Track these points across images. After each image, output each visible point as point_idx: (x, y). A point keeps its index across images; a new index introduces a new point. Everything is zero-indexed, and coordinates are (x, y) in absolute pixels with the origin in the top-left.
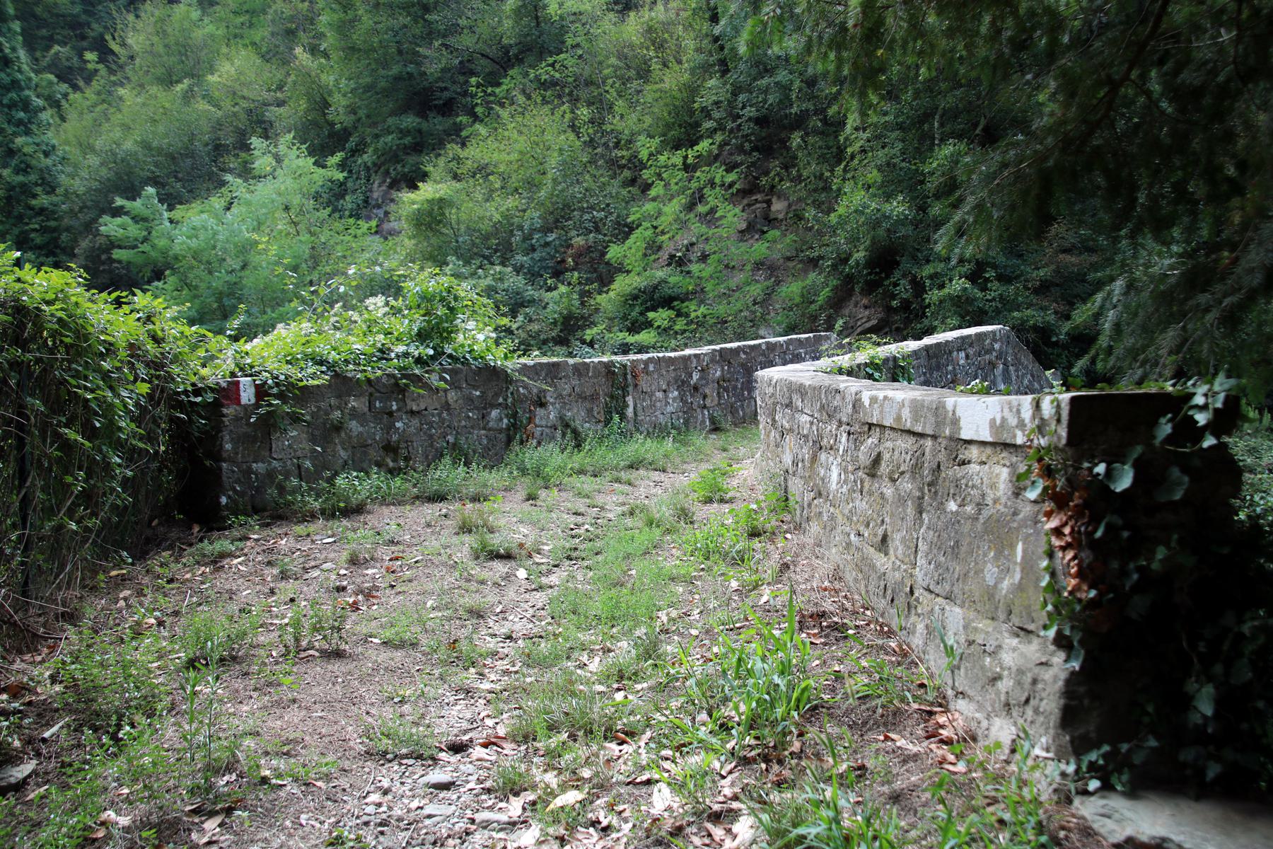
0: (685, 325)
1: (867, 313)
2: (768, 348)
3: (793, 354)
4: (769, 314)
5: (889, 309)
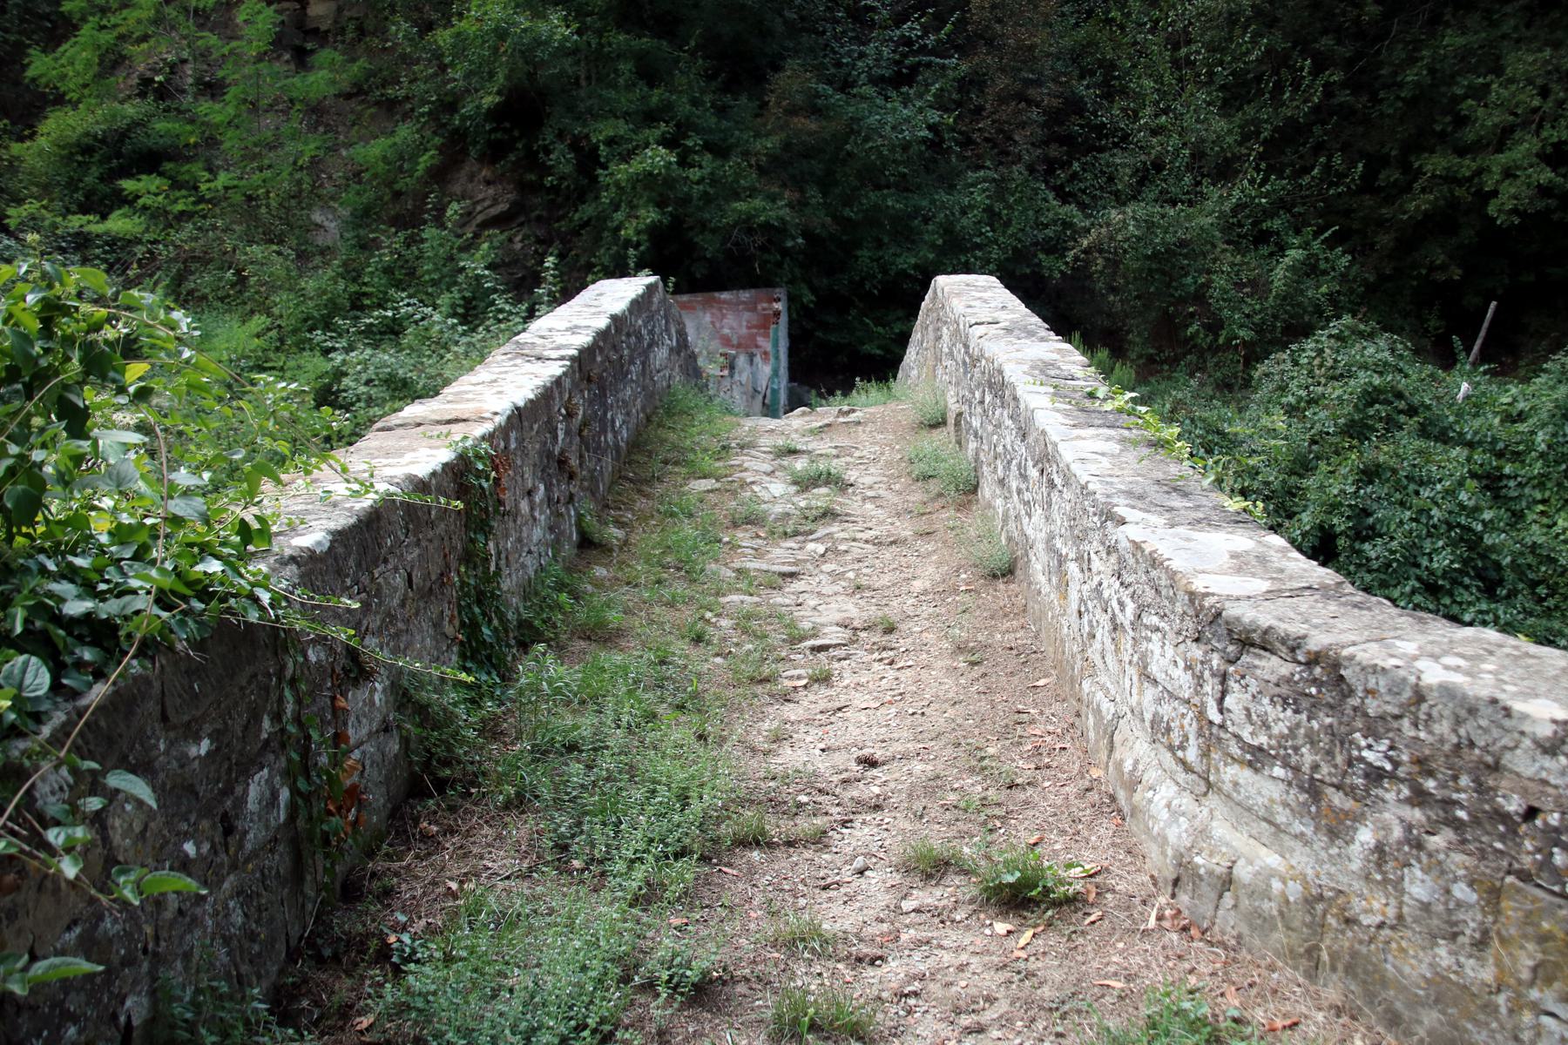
1: (491, 191)
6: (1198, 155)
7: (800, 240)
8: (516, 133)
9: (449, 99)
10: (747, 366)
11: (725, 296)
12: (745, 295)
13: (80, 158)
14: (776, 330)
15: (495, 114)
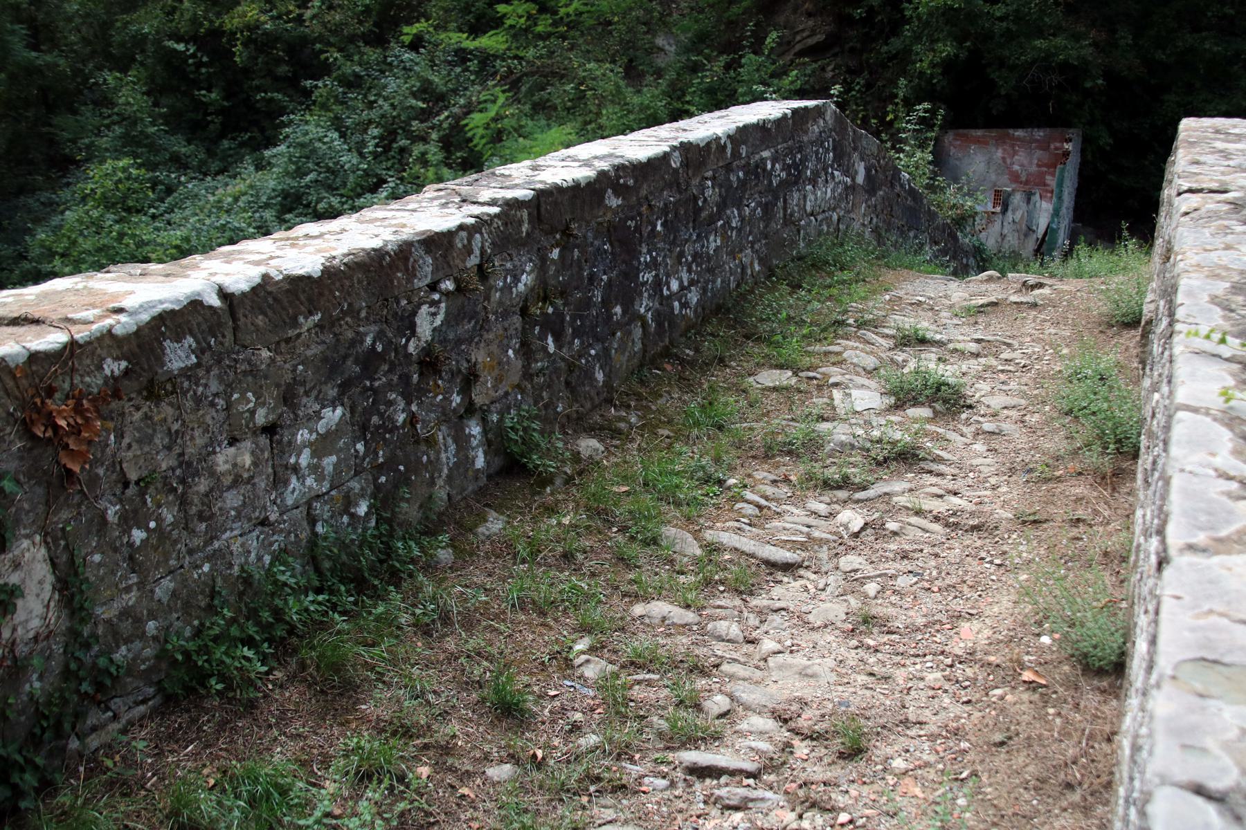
0: (551, 25)
1: (811, 23)
2: (686, 164)
3: (747, 168)
4: (670, 15)
5: (845, 21)
6: (1106, 554)
7: (1100, 82)
10: (1024, 206)
11: (1019, 133)
12: (1039, 134)
14: (1063, 171)
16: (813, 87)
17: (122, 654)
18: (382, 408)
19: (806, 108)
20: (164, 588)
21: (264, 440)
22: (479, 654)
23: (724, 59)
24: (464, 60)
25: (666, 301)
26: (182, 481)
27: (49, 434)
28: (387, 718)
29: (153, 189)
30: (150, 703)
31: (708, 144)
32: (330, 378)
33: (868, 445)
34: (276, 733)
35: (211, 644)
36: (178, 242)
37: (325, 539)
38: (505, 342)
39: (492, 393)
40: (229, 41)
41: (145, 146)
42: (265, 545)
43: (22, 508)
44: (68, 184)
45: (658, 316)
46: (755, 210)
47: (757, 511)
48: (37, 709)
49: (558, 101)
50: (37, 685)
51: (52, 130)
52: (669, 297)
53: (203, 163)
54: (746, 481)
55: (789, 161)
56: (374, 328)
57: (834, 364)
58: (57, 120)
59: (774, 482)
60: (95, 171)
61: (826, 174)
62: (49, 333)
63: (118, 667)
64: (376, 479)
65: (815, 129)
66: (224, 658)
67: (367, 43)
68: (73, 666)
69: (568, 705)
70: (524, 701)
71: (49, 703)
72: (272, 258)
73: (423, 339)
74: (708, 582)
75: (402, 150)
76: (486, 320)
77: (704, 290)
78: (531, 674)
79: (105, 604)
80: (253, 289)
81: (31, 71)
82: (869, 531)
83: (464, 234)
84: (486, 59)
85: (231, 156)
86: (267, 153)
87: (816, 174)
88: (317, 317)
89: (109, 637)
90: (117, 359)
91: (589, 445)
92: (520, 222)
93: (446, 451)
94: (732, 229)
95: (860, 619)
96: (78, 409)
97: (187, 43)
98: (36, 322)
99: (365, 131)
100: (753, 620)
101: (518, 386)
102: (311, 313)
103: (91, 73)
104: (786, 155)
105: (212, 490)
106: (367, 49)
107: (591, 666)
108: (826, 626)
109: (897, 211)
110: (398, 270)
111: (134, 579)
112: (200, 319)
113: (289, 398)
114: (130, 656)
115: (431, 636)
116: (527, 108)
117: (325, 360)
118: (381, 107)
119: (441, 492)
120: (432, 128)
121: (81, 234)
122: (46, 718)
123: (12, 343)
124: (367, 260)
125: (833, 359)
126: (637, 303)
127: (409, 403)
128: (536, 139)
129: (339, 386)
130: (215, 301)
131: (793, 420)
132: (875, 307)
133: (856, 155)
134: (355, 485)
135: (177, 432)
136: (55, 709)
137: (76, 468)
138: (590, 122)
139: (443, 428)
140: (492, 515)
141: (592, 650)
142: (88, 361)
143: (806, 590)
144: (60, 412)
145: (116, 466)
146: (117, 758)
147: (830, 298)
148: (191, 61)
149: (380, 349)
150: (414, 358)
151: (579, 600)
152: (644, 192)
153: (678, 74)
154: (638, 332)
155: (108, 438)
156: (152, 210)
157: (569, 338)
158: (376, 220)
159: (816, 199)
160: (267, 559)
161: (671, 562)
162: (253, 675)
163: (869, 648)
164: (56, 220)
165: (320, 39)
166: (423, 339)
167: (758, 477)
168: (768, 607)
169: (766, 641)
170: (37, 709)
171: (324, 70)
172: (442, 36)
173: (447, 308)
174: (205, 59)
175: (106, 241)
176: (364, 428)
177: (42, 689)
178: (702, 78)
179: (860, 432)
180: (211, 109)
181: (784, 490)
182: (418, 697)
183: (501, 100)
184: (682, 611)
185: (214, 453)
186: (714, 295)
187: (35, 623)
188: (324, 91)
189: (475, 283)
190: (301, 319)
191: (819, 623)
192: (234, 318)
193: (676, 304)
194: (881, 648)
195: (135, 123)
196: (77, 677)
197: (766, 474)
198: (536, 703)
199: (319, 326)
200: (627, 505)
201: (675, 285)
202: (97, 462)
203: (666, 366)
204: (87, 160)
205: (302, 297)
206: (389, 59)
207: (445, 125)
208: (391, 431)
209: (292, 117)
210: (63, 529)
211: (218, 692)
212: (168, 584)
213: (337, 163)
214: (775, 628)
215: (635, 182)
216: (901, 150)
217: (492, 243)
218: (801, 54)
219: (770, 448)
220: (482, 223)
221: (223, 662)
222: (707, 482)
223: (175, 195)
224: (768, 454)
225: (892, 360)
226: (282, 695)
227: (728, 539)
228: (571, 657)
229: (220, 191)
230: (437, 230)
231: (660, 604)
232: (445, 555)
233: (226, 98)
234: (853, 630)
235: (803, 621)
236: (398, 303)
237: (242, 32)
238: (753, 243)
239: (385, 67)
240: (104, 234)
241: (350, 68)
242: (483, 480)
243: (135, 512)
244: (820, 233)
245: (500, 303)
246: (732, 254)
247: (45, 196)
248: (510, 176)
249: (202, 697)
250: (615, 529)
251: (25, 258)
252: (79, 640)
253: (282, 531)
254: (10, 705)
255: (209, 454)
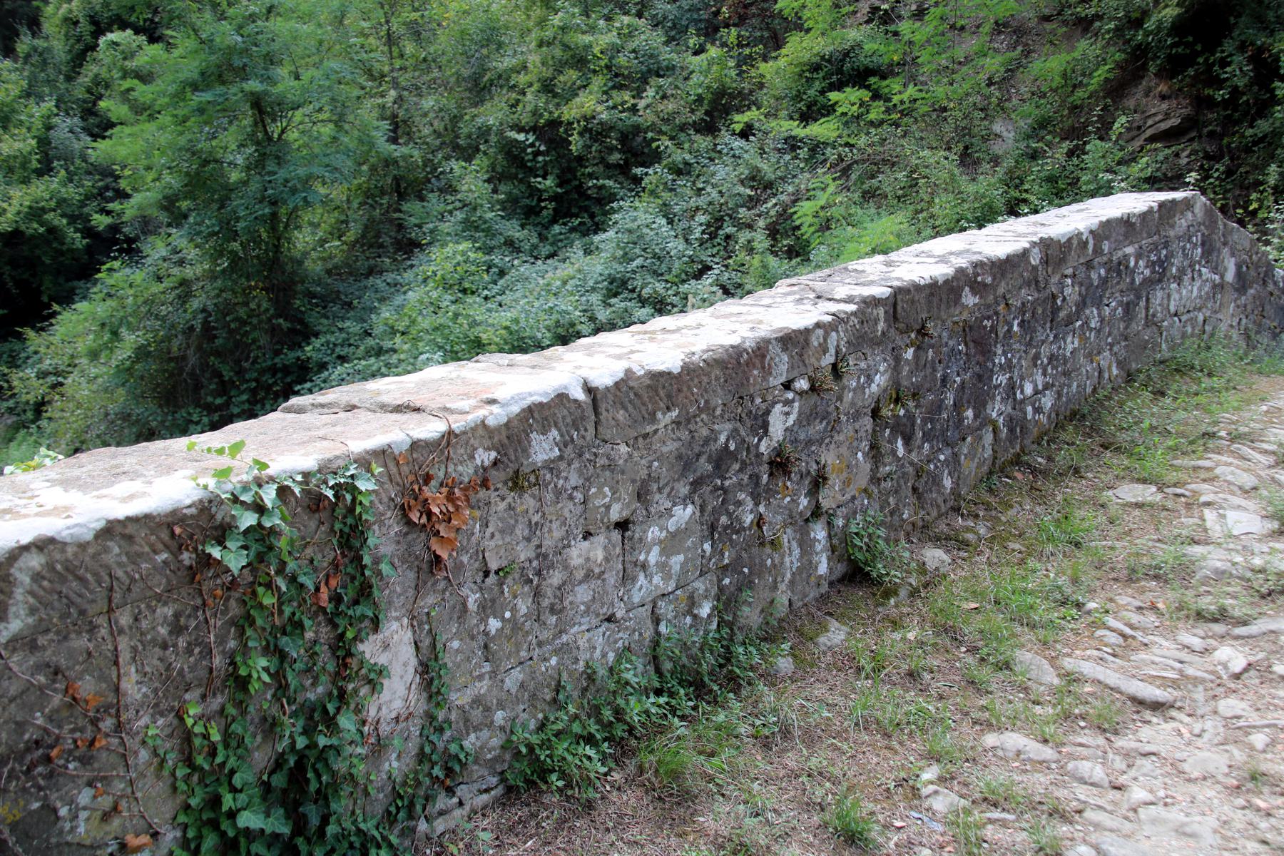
1: (1164, 106)
2: (1046, 261)
4: (1009, 100)
5: (1203, 103)
8: (1199, 47)
9: (1135, 15)
13: (807, 74)
15: (1179, 28)
16: (1165, 174)
17: (470, 742)
18: (731, 508)
19: (1173, 201)
20: (513, 679)
21: (616, 535)
22: (820, 774)
23: (1066, 145)
24: (794, 148)
25: (1019, 405)
26: (539, 573)
27: (424, 520)
28: (726, 834)
29: (488, 271)
30: (493, 793)
31: (1070, 240)
32: (683, 475)
33: (1249, 574)
34: (614, 838)
35: (553, 739)
36: (508, 323)
37: (669, 639)
38: (855, 444)
39: (839, 496)
40: (566, 131)
41: (483, 231)
42: (611, 642)
43: (395, 591)
44: (412, 266)
45: (1010, 422)
46: (1116, 309)
47: (1121, 640)
48: (394, 788)
49: (888, 190)
50: (395, 764)
51: (402, 215)
52: (1022, 401)
53: (535, 247)
54: (1110, 606)
55: (1153, 258)
56: (729, 426)
57: (1204, 481)
58: (406, 206)
59: (1139, 608)
60: (436, 253)
61: (1193, 271)
62: (429, 421)
63: (467, 754)
64: (720, 581)
65: (1182, 223)
66: (566, 754)
67: (697, 131)
68: (427, 750)
69: (916, 839)
70: (869, 830)
71: (404, 784)
72: (632, 352)
73: (775, 439)
74: (1067, 716)
75: (728, 237)
76: (838, 420)
77: (1059, 394)
78: (876, 801)
79: (459, 690)
80: (617, 384)
81: (389, 162)
82: (1252, 673)
83: (820, 332)
84: (816, 147)
85: (561, 241)
86: (596, 238)
87: (1182, 271)
88: (675, 413)
89: (461, 724)
90: (488, 449)
91: (934, 556)
92: (876, 321)
93: (790, 555)
94: (1091, 329)
95: (1246, 775)
96: (450, 497)
97: (527, 132)
98: (417, 410)
99: (692, 217)
100: (1120, 764)
101: (865, 491)
102: (668, 409)
103: (440, 163)
104: (1151, 251)
105: (564, 583)
106: (698, 138)
107: (940, 798)
108: (1205, 779)
109: (1269, 311)
110: (755, 367)
111: (487, 667)
112: (565, 412)
113: (642, 495)
114: (479, 744)
115: (771, 749)
116: (856, 196)
117: (680, 457)
118: (709, 194)
119: (782, 598)
120: (759, 216)
121: (421, 313)
122: (401, 798)
123: (398, 431)
124: (726, 357)
125: (1203, 475)
126: (989, 407)
127: (757, 504)
128: (865, 228)
129: (692, 484)
130: (580, 395)
131: (1159, 540)
132: (1252, 417)
133: (1226, 251)
134: (700, 586)
135: (536, 524)
136: (410, 790)
137: (444, 555)
138: (922, 211)
139: (788, 531)
140: (833, 624)
141: (941, 780)
142: (462, 451)
143: (1180, 734)
144: (434, 499)
145: (480, 555)
146: (461, 845)
147: (1197, 406)
148: (529, 150)
149: (732, 447)
150: (766, 458)
151: (923, 725)
152: (1001, 291)
153: (1017, 162)
154: (988, 437)
155: (474, 527)
156: (486, 292)
157: (919, 442)
158: (731, 315)
159: (1181, 299)
160: (611, 656)
161: (1026, 690)
162: (592, 775)
163: (1259, 810)
164: (398, 300)
165: (652, 127)
166: (775, 439)
167: (1121, 602)
168: (1136, 750)
169: (1135, 789)
170: (394, 788)
171: (654, 157)
172: (774, 124)
173: (800, 407)
174: (543, 148)
175: (442, 321)
176: (713, 528)
177: (399, 770)
178: (1042, 166)
179: (1239, 559)
180: (545, 196)
181: (1150, 619)
182: (758, 815)
183: (831, 189)
184: (1040, 746)
185: (570, 546)
186: (1069, 401)
187: (398, 704)
188: (653, 179)
189: (830, 382)
190: (659, 415)
191: (1195, 774)
192: (597, 413)
193: (1029, 409)
194: (1274, 812)
195: (475, 209)
196: (430, 760)
197: (1130, 599)
198: (881, 833)
199: (677, 423)
200: (978, 622)
201: (1029, 389)
202: (463, 549)
203: (1016, 474)
204: (430, 243)
205: (662, 393)
206: (719, 148)
207: (773, 213)
208: (738, 532)
209: (622, 203)
210: (428, 614)
211: (560, 790)
212: (517, 675)
213: (664, 249)
214: (1145, 775)
215: (994, 279)
216: (1267, 243)
217: (848, 342)
218: (1152, 139)
219: (1134, 571)
220: (839, 320)
221: (564, 759)
222: (1063, 604)
223: (507, 277)
224: (1131, 578)
225: (1273, 478)
226: (620, 797)
227: (1088, 668)
228: (919, 786)
229: (550, 274)
230: (795, 327)
231: (1014, 735)
232: (785, 664)
233: (559, 185)
234: (1238, 787)
235: (1176, 769)
236: (752, 401)
237: (579, 122)
238: (1111, 345)
239: (715, 154)
240: (440, 315)
241: (679, 156)
242: (825, 588)
243: (493, 601)
244: (1184, 336)
245: (853, 404)
246: (1090, 357)
247: (390, 277)
248: (863, 271)
249: (542, 792)
250: (963, 649)
251: (370, 335)
252: (434, 724)
253: (627, 628)
254: (371, 781)
255: (564, 547)
